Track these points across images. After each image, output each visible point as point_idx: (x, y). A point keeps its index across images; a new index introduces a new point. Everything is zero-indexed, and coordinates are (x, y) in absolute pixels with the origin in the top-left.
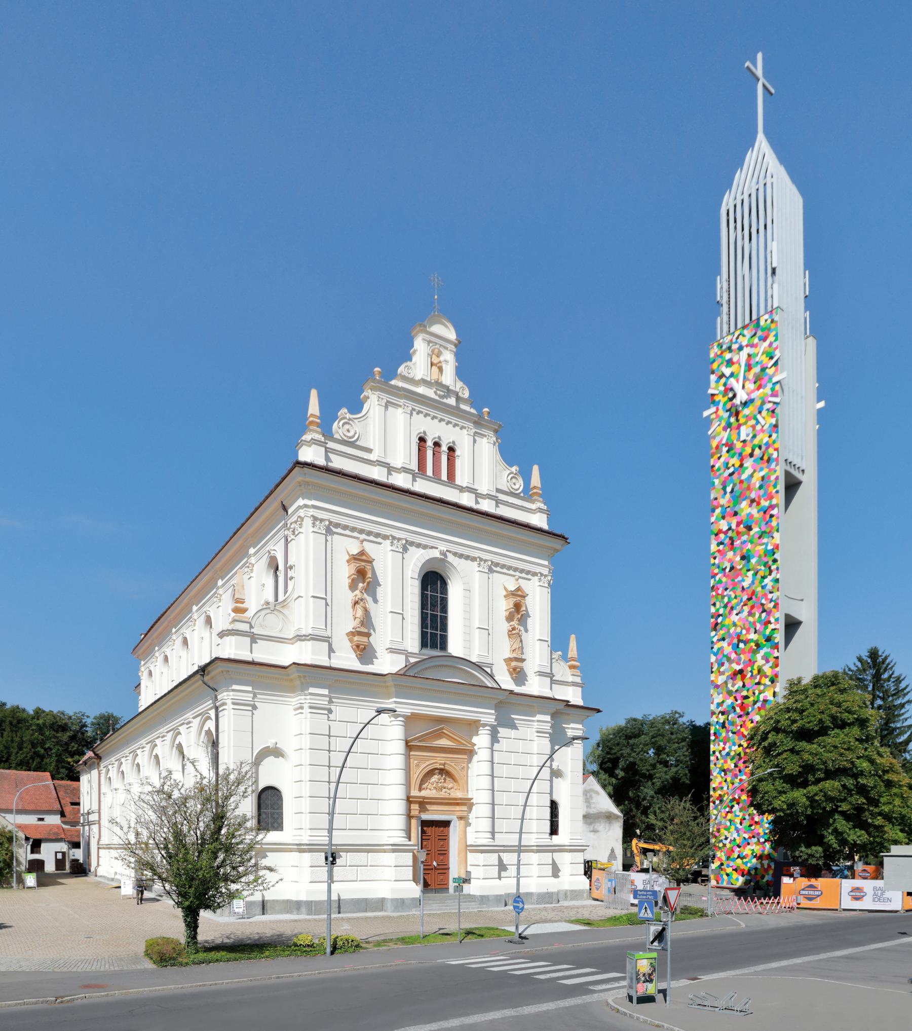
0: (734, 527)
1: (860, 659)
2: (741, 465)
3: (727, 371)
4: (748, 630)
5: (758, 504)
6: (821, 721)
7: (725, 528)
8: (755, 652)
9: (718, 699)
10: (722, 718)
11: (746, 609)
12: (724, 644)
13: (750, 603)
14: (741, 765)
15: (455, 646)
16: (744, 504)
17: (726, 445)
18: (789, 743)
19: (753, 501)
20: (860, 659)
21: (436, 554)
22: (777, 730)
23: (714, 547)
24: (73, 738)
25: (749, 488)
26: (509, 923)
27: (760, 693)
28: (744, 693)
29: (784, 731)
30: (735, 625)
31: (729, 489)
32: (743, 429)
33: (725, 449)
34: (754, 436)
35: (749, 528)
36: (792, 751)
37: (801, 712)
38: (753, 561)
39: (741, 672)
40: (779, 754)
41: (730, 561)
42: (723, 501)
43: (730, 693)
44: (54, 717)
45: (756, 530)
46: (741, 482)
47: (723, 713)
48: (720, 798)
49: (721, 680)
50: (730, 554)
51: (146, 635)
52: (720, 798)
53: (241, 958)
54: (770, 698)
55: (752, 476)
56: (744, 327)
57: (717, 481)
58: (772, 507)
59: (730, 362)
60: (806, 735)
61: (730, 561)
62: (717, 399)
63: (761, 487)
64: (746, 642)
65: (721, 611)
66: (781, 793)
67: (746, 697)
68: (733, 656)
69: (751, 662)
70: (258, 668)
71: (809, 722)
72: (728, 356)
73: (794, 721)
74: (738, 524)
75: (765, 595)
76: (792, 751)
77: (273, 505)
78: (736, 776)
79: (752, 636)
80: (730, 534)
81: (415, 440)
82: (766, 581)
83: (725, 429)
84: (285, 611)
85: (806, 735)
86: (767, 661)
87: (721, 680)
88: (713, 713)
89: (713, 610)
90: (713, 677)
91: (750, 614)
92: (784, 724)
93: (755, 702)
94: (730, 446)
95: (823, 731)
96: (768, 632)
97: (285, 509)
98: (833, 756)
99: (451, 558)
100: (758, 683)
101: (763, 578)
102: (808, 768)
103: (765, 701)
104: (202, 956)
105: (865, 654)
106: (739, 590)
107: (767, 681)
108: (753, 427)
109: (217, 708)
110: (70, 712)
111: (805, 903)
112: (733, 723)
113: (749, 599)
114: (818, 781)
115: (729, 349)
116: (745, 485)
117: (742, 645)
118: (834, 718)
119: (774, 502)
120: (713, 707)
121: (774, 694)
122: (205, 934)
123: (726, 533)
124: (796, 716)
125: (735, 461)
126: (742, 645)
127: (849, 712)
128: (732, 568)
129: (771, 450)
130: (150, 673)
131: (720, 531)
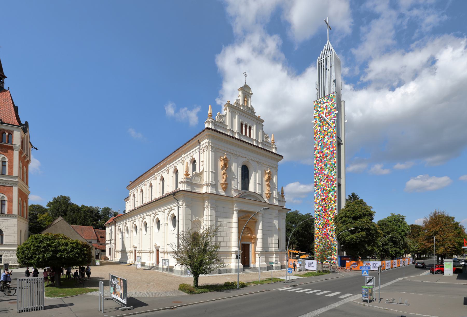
0: (322, 155)
1: (349, 196)
2: (324, 138)
3: (319, 110)
4: (326, 187)
5: (330, 149)
6: (360, 214)
7: (319, 156)
8: (329, 193)
9: (317, 207)
10: (318, 213)
11: (326, 180)
12: (319, 191)
13: (327, 179)
14: (324, 227)
15: (251, 188)
16: (325, 149)
17: (319, 131)
18: (350, 220)
19: (328, 148)
20: (349, 196)
21: (246, 159)
22: (346, 217)
23: (315, 162)
24: (96, 215)
25: (327, 145)
26: (283, 276)
27: (331, 205)
28: (325, 205)
29: (348, 217)
30: (322, 185)
31: (320, 145)
32: (324, 127)
33: (319, 133)
34: (328, 129)
35: (327, 156)
36: (351, 223)
37: (354, 211)
38: (328, 166)
39: (324, 199)
40: (347, 224)
41: (320, 166)
42: (318, 148)
43: (321, 205)
44: (89, 208)
45: (329, 157)
46: (324, 143)
47: (318, 211)
48: (318, 237)
49: (318, 201)
50: (320, 164)
51: (132, 183)
52: (318, 237)
53: (207, 292)
54: (334, 207)
55: (327, 141)
56: (325, 97)
57: (316, 142)
58: (334, 150)
59: (320, 107)
60: (355, 218)
61: (320, 166)
62: (316, 118)
63: (330, 144)
64: (326, 190)
65: (318, 181)
66: (348, 235)
67: (326, 207)
68: (322, 194)
69: (327, 196)
70: (192, 193)
71: (356, 214)
72: (320, 105)
73: (352, 214)
74: (323, 155)
75: (332, 176)
76: (351, 223)
77: (195, 141)
78: (323, 230)
79: (328, 188)
80: (320, 158)
81: (240, 124)
82: (332, 172)
83: (319, 127)
84: (201, 176)
85: (355, 218)
86: (333, 196)
87: (318, 201)
88: (315, 211)
89: (315, 180)
90: (315, 200)
91: (327, 182)
92: (348, 215)
93: (329, 208)
94: (320, 132)
95: (360, 217)
96: (333, 187)
97: (200, 143)
98: (364, 225)
99: (250, 161)
100: (330, 203)
101: (331, 171)
102: (356, 228)
103: (332, 208)
104: (201, 290)
105: (351, 195)
106: (323, 174)
107: (333, 202)
108: (328, 127)
109: (178, 207)
110: (94, 206)
111: (353, 268)
112: (322, 215)
113: (327, 177)
114: (359, 232)
115: (320, 103)
116: (325, 144)
117: (324, 191)
118: (363, 213)
119: (335, 149)
120: (315, 209)
121: (335, 206)
122: (200, 283)
123: (319, 157)
124: (352, 212)
125: (322, 136)
126: (324, 191)
127: (367, 212)
128: (321, 168)
129: (333, 134)
130: (134, 195)
131: (317, 157)
